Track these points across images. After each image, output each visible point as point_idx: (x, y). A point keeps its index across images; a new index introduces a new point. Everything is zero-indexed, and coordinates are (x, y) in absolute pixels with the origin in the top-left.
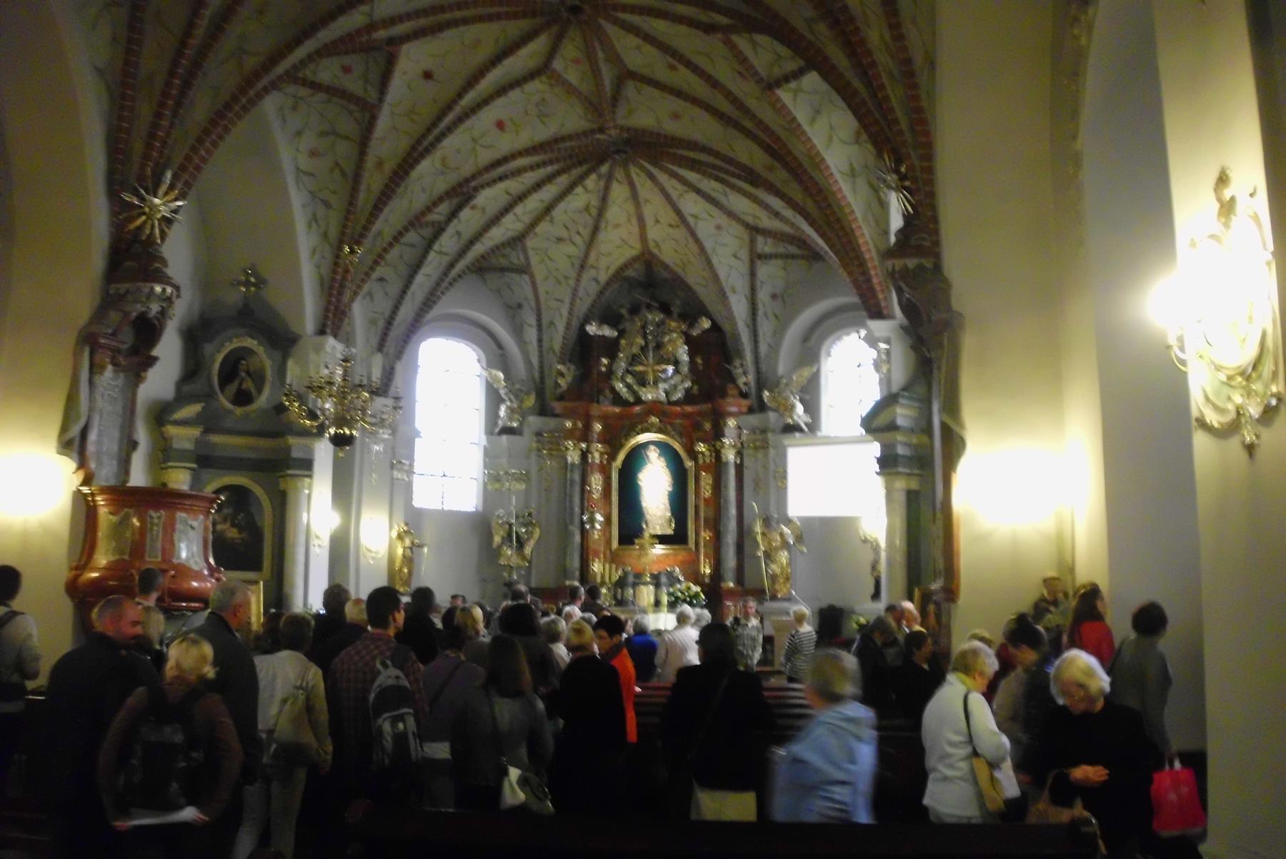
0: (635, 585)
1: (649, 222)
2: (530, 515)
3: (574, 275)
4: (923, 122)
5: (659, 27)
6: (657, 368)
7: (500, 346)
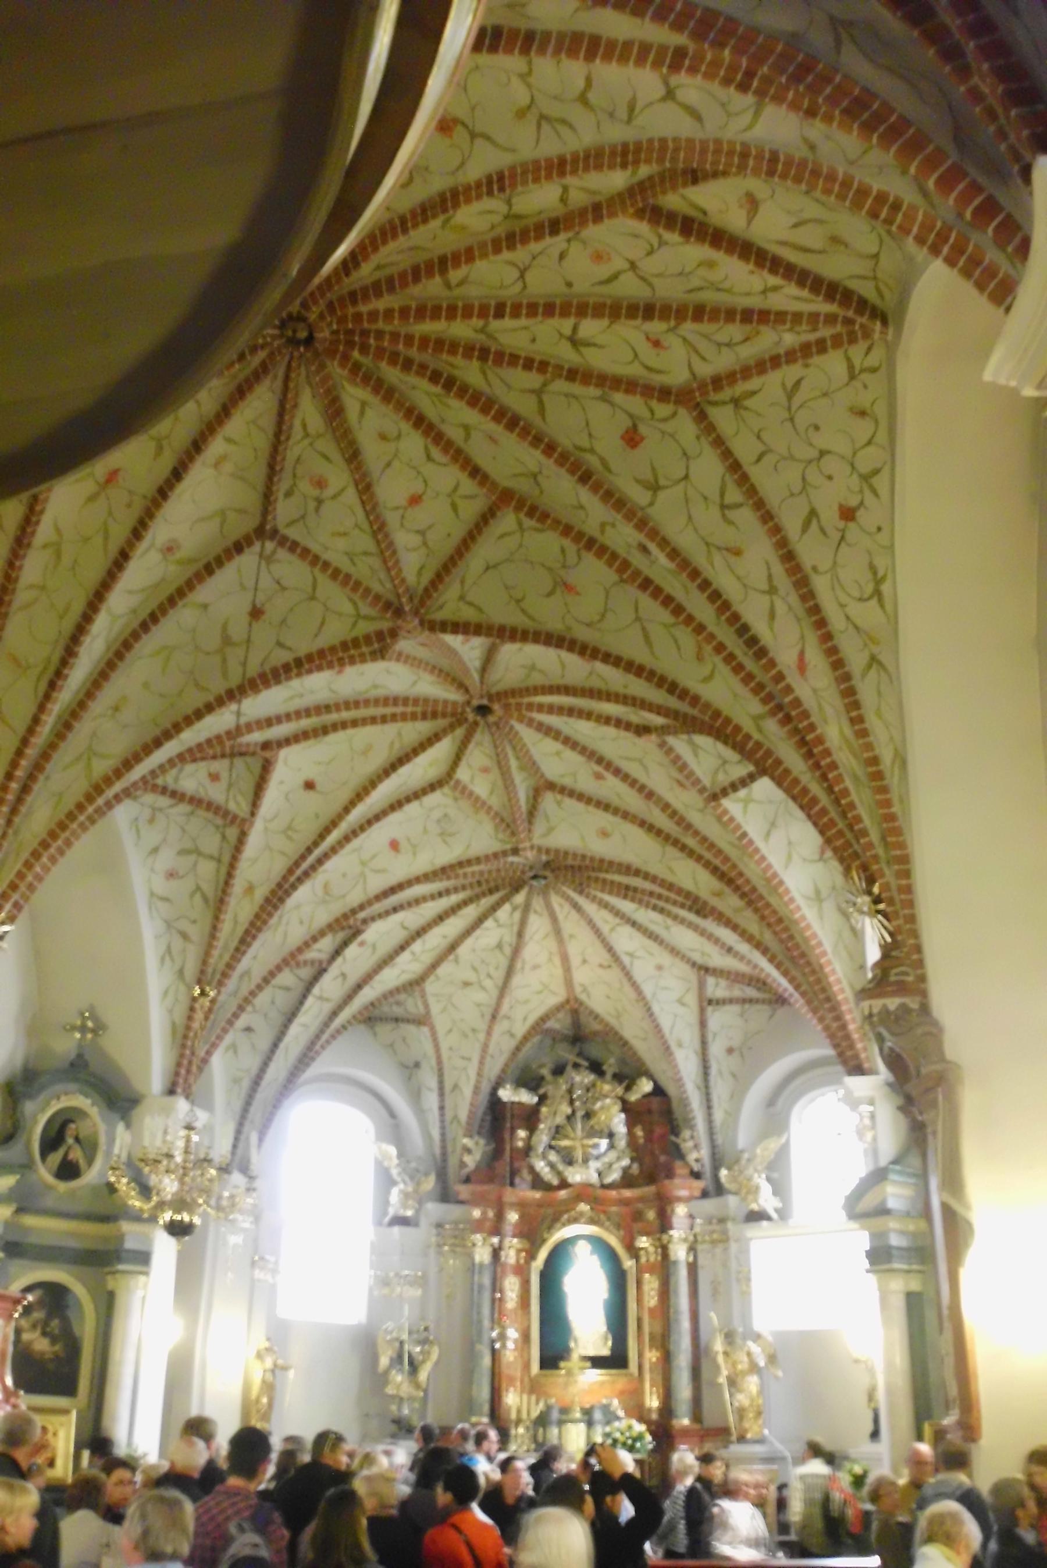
0: (561, 1423)
1: (575, 961)
2: (426, 1329)
3: (482, 1025)
4: (898, 832)
5: (583, 729)
6: (591, 1142)
7: (392, 1115)
